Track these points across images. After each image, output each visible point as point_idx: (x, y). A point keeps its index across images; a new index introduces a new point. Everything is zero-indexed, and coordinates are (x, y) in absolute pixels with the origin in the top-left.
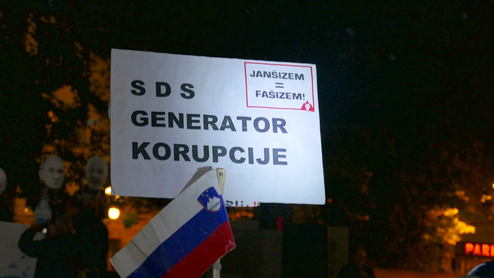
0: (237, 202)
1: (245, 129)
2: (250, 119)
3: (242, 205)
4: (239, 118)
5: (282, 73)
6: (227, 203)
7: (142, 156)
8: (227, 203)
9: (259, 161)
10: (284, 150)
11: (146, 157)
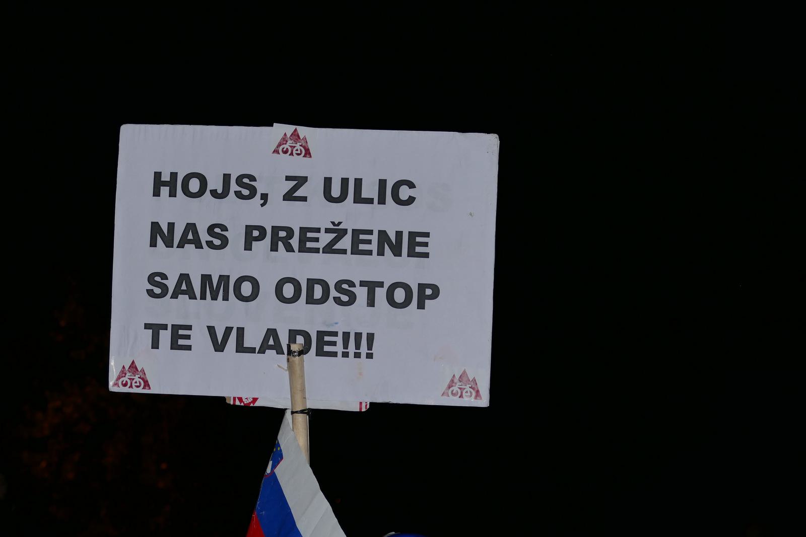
1: (371, 302)
2: (381, 284)
4: (362, 283)
5: (344, 252)
9: (214, 193)
10: (427, 235)
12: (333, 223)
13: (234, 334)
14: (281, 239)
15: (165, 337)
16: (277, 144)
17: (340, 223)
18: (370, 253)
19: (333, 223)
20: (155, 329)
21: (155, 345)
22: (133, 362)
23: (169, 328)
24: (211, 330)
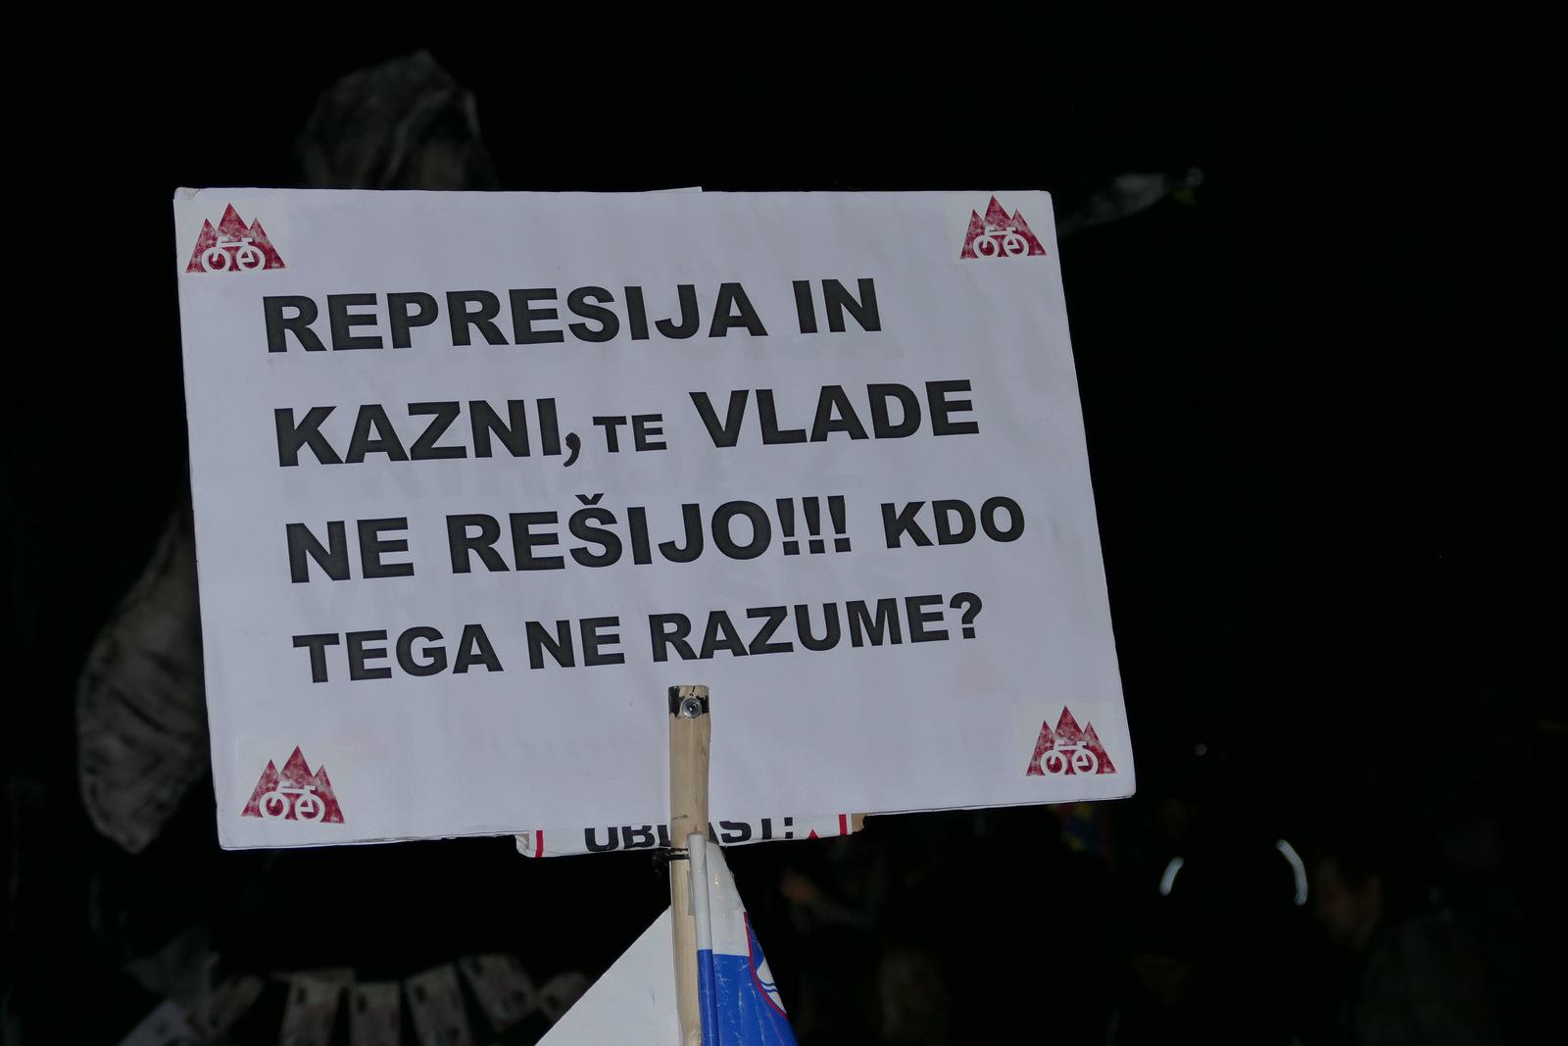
0: (766, 824)
3: (789, 835)
6: (726, 832)
7: (500, 442)
8: (726, 832)
11: (921, 540)
14: (291, 324)
15: (337, 657)
16: (964, 237)
18: (375, 343)
20: (316, 644)
21: (320, 674)
22: (1066, 712)
23: (343, 639)
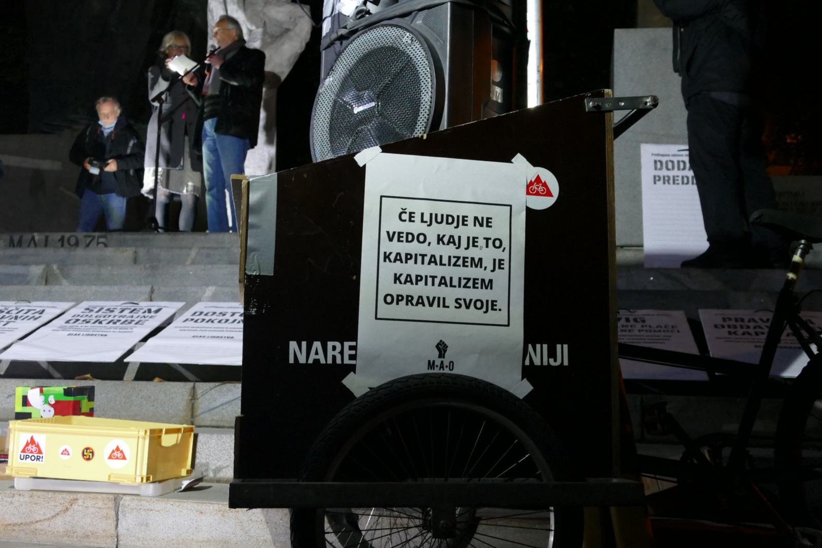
12: (402, 209)
13: (396, 234)
17: (405, 209)
19: (402, 209)
24: (388, 233)
